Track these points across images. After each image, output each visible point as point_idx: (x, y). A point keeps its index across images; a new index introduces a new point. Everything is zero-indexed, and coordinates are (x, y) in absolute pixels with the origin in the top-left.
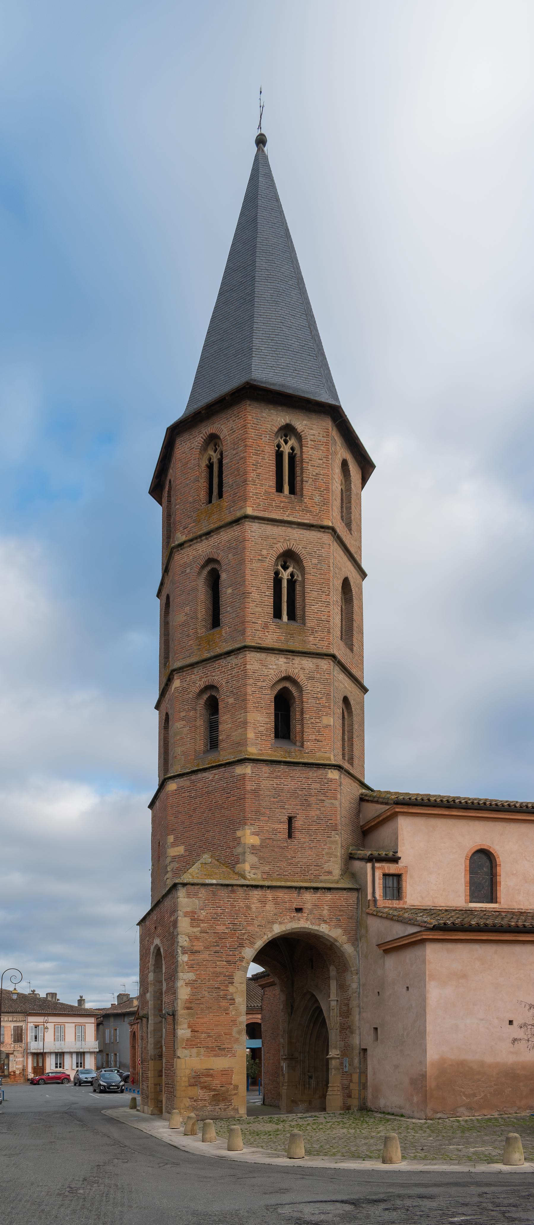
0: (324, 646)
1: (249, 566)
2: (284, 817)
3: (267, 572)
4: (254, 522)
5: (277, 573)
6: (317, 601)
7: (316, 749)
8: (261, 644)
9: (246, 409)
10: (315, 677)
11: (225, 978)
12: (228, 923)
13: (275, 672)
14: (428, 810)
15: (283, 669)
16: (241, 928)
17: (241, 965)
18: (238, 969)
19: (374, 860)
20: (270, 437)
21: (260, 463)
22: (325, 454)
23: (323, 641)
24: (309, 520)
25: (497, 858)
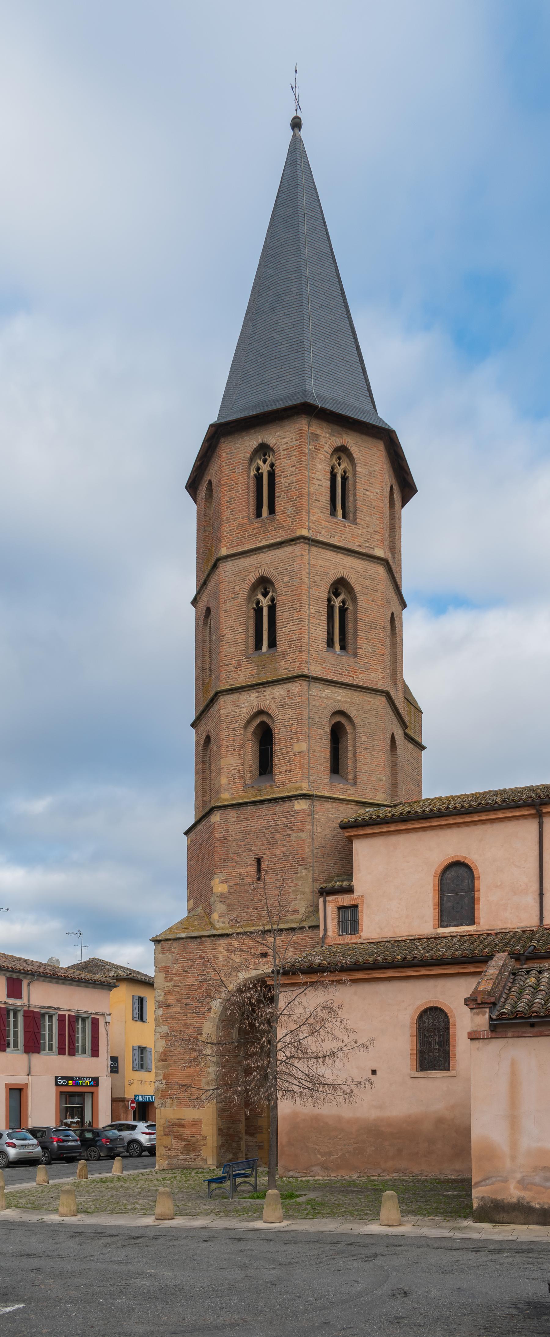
0: (295, 667)
1: (223, 608)
2: (250, 859)
3: (240, 607)
4: (227, 561)
6: (288, 621)
7: (287, 780)
8: (234, 685)
10: (286, 704)
12: (198, 975)
13: (247, 710)
14: (382, 828)
15: (254, 704)
17: (209, 1015)
18: (206, 1019)
19: (324, 894)
20: (243, 466)
22: (298, 458)
23: (295, 662)
25: (475, 870)
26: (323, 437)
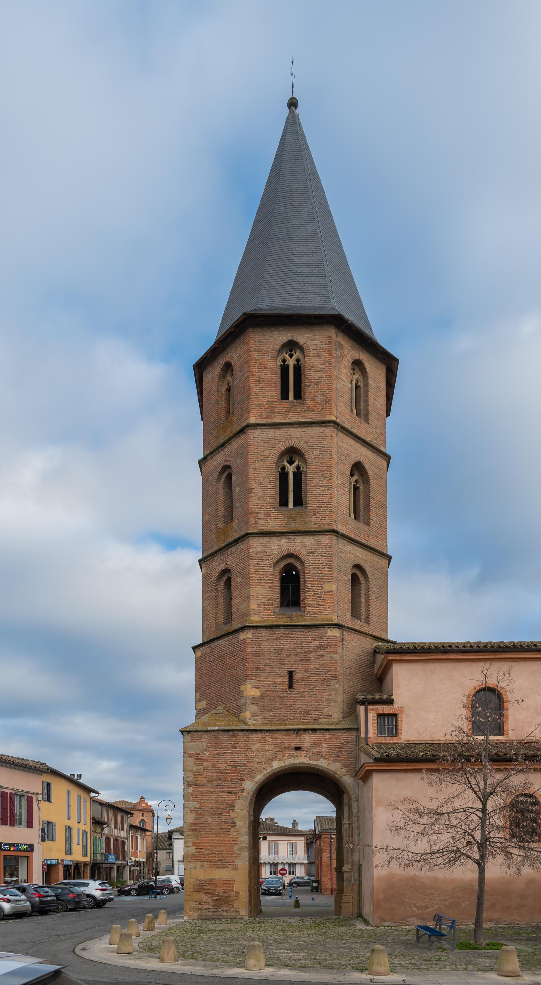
0: (326, 524)
1: (251, 466)
4: (256, 429)
5: (283, 468)
9: (249, 336)
11: (227, 806)
13: (277, 551)
14: (424, 656)
15: (285, 547)
16: (241, 765)
19: (367, 703)
20: (272, 355)
21: (263, 379)
22: (328, 359)
23: (325, 519)
24: (311, 418)
26: (346, 348)
